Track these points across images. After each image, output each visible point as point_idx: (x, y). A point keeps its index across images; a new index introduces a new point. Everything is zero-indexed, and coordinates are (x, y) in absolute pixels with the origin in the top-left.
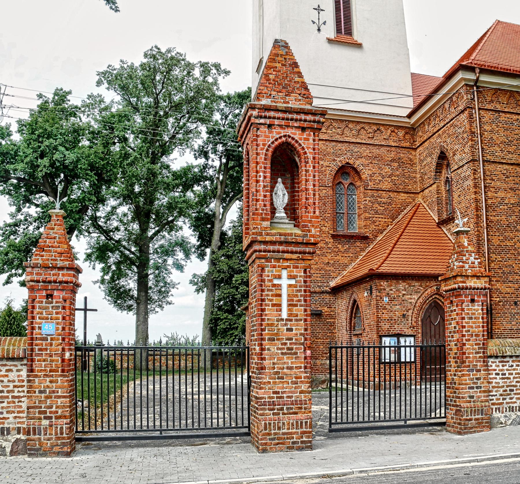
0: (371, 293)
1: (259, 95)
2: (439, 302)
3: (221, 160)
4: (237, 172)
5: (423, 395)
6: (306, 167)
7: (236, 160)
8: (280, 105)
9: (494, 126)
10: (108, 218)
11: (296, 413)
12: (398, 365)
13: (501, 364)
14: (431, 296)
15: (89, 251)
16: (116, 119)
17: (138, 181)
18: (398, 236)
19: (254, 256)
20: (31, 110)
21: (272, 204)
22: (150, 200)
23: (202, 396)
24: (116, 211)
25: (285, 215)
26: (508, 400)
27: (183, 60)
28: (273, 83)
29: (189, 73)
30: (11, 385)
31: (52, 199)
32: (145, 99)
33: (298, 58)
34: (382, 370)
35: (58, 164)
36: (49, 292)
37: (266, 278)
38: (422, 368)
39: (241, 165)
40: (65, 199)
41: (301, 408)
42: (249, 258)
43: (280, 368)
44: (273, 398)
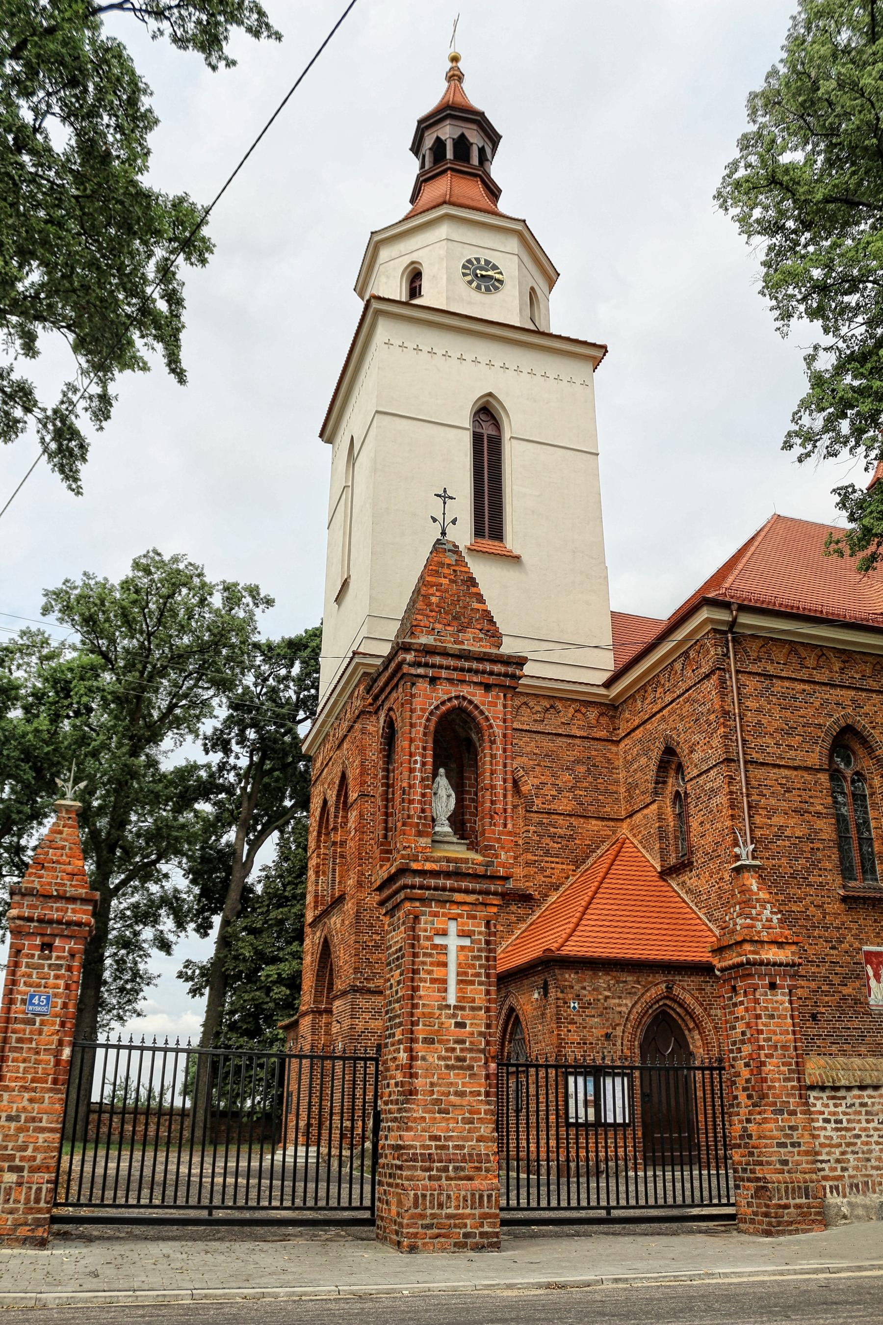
0: (546, 994)
2: (671, 1012)
3: (251, 757)
6: (491, 749)
7: (279, 758)
8: (450, 645)
11: (470, 1179)
13: (831, 1102)
14: (657, 1002)
18: (590, 894)
19: (401, 895)
23: (230, 1180)
25: (450, 830)
28: (437, 609)
36: (47, 939)
41: (479, 1169)
43: (443, 1094)
44: (429, 1147)
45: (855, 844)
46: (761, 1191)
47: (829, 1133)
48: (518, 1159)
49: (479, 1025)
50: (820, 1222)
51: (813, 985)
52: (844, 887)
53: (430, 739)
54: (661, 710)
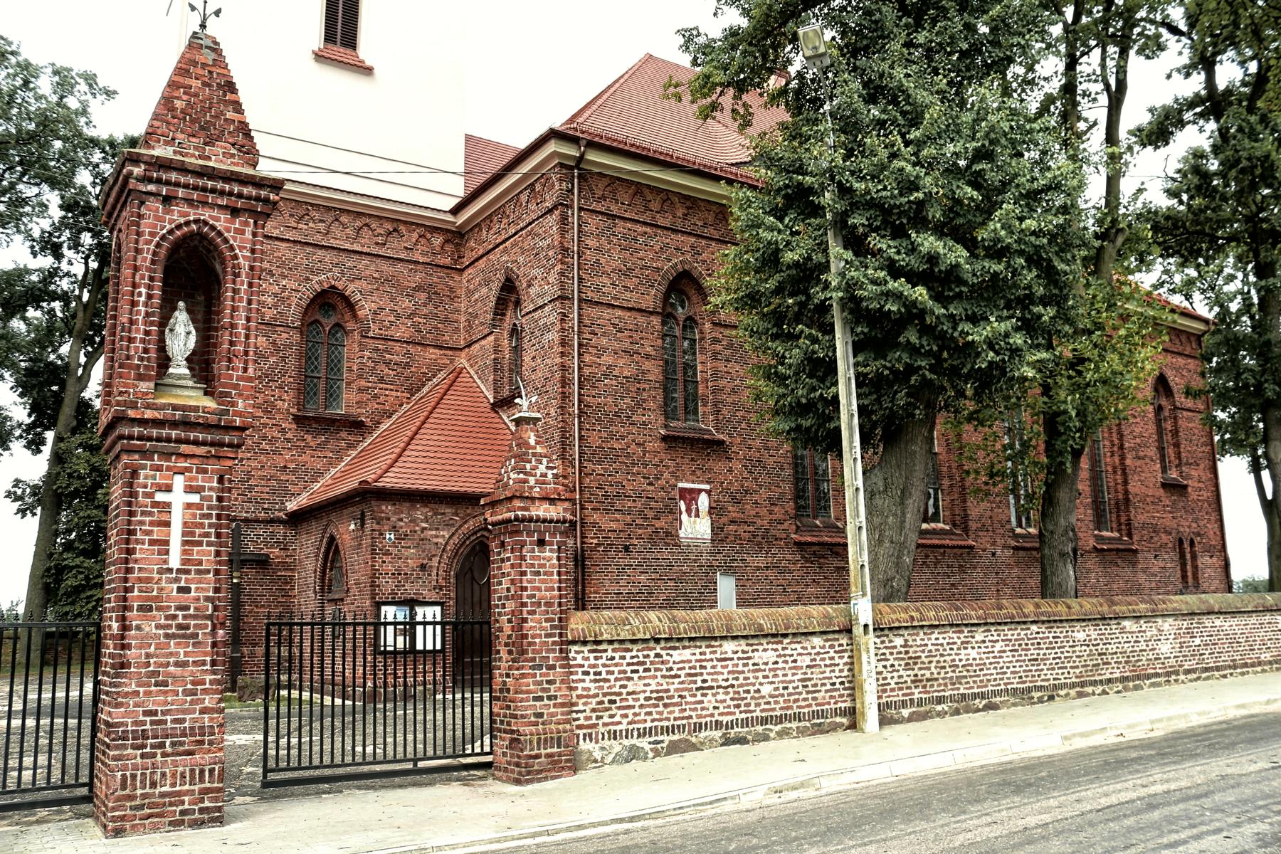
3: (86, 264)
5: (459, 711)
6: (234, 282)
8: (192, 160)
12: (410, 658)
13: (592, 656)
14: (475, 533)
19: (118, 448)
21: (162, 349)
25: (187, 372)
26: (606, 720)
28: (181, 116)
29: (26, 83)
34: (380, 666)
37: (141, 490)
38: (458, 660)
41: (202, 742)
43: (161, 665)
44: (144, 723)
45: (680, 386)
46: (514, 743)
47: (587, 685)
48: (333, 684)
49: (207, 590)
50: (570, 768)
52: (666, 426)
53: (159, 268)
54: (504, 241)
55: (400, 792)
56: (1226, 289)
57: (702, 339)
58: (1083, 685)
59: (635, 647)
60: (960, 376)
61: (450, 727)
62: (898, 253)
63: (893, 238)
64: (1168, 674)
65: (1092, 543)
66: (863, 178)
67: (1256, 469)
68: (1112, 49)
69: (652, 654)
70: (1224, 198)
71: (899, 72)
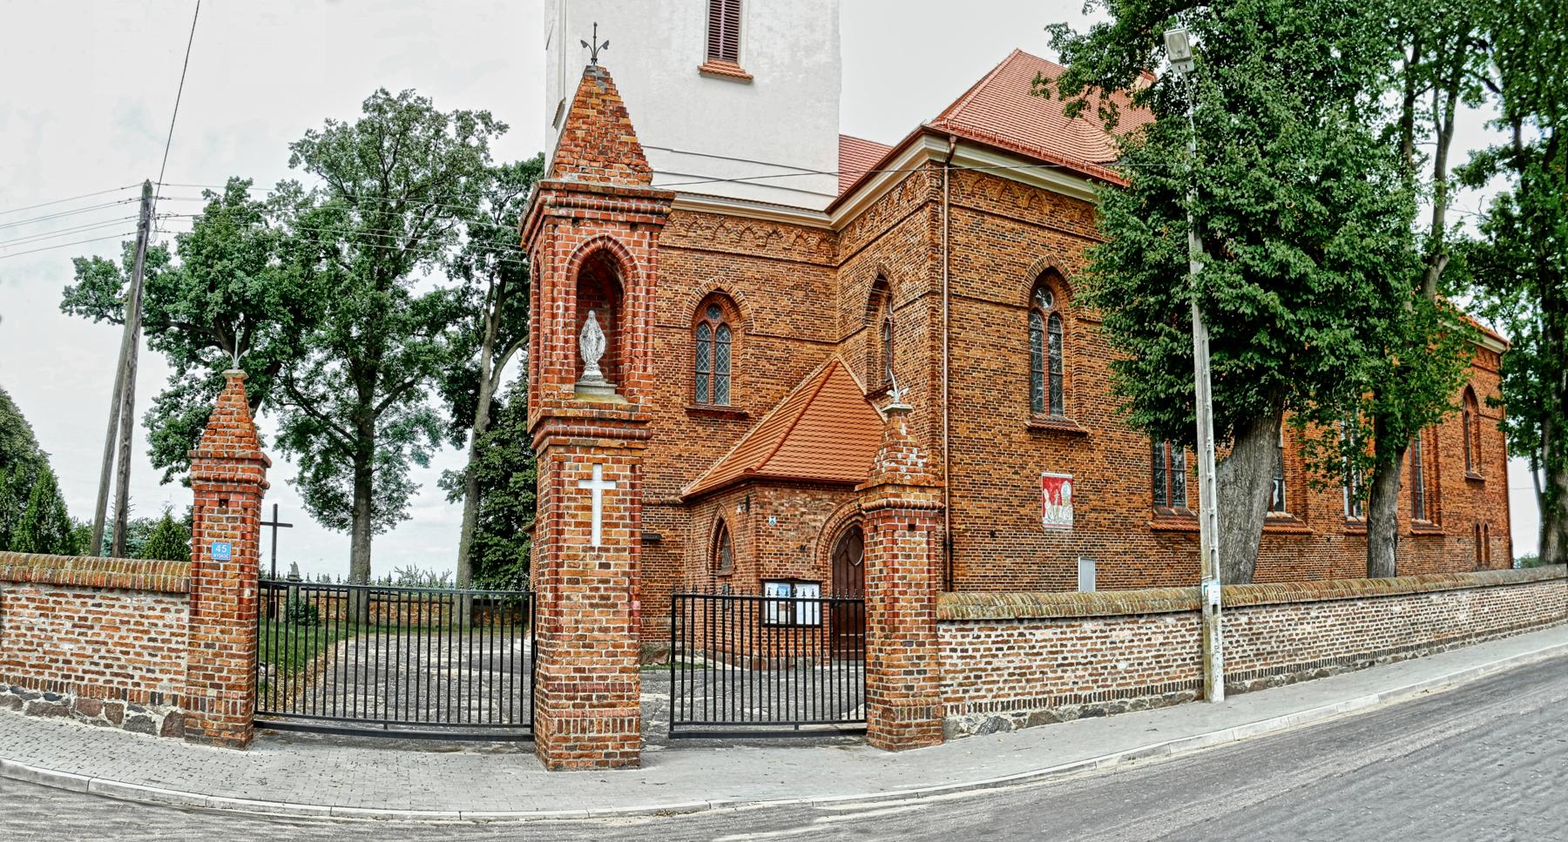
0: (748, 508)
1: (557, 166)
4: (520, 300)
8: (595, 183)
9: (972, 237)
10: (310, 380)
11: (613, 706)
15: (282, 433)
16: (321, 219)
17: (357, 319)
19: (546, 442)
20: (195, 217)
21: (578, 354)
22: (376, 350)
23: (455, 671)
24: (322, 370)
26: (972, 693)
27: (428, 110)
29: (438, 132)
30: (168, 631)
31: (227, 354)
32: (366, 183)
33: (626, 100)
34: (765, 637)
35: (235, 299)
38: (835, 635)
39: (526, 288)
40: (246, 353)
41: (621, 697)
42: (537, 445)
43: (588, 630)
44: (574, 678)
45: (1045, 379)
51: (994, 506)
53: (573, 283)
55: (783, 751)
56: (1520, 317)
57: (1067, 334)
58: (1398, 650)
59: (1000, 627)
60: (1304, 378)
61: (827, 696)
62: (1253, 258)
63: (1249, 244)
64: (1463, 638)
65: (1410, 529)
66: (1223, 184)
67: (1534, 468)
68: (1443, 93)
69: (1016, 633)
70: (1523, 240)
71: (1258, 85)
